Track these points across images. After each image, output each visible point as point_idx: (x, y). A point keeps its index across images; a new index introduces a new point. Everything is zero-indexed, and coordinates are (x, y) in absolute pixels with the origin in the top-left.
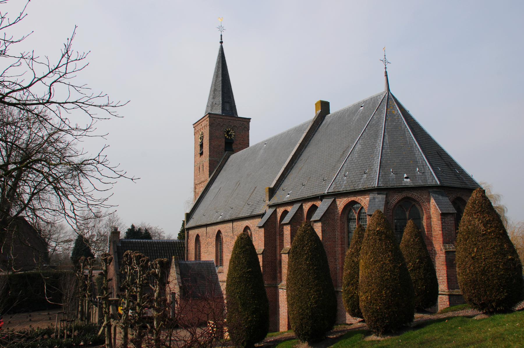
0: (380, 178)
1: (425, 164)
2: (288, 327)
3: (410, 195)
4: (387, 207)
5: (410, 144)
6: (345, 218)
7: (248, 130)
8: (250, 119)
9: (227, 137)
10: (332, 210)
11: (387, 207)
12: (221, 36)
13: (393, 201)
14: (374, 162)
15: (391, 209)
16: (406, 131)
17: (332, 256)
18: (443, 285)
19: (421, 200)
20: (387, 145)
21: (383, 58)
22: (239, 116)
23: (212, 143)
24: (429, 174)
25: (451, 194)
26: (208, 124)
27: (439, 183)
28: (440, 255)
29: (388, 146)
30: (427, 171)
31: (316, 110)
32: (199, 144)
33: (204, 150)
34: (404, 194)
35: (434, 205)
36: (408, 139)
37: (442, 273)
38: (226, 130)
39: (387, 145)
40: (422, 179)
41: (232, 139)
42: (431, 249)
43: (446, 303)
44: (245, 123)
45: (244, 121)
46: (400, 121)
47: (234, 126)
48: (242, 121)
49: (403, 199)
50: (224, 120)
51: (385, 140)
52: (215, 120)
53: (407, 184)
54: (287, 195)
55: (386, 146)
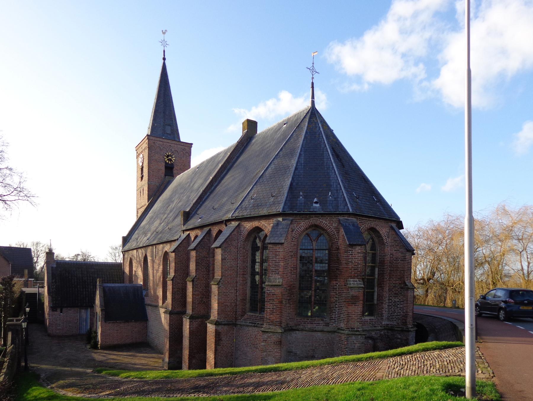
1: (339, 189)
2: (189, 357)
4: (292, 235)
5: (327, 165)
6: (249, 246)
7: (190, 155)
8: (192, 144)
9: (167, 161)
10: (235, 236)
11: (292, 235)
12: (164, 51)
13: (299, 229)
14: (284, 184)
15: (296, 238)
16: (325, 150)
17: (233, 287)
18: (344, 323)
19: (329, 229)
20: (301, 166)
21: (310, 66)
23: (151, 166)
24: (342, 199)
25: (364, 223)
26: (147, 147)
27: (351, 210)
28: (343, 291)
29: (302, 167)
30: (340, 197)
31: (243, 131)
32: (141, 167)
33: (144, 174)
34: (314, 220)
35: (342, 236)
36: (325, 160)
37: (344, 310)
38: (166, 154)
39: (301, 166)
41: (173, 164)
42: (336, 283)
43: (344, 343)
44: (186, 148)
45: (186, 146)
46: (320, 140)
48: (184, 146)
49: (310, 227)
50: (164, 143)
52: (154, 142)
53: (315, 210)
54: (199, 219)
55: (300, 167)
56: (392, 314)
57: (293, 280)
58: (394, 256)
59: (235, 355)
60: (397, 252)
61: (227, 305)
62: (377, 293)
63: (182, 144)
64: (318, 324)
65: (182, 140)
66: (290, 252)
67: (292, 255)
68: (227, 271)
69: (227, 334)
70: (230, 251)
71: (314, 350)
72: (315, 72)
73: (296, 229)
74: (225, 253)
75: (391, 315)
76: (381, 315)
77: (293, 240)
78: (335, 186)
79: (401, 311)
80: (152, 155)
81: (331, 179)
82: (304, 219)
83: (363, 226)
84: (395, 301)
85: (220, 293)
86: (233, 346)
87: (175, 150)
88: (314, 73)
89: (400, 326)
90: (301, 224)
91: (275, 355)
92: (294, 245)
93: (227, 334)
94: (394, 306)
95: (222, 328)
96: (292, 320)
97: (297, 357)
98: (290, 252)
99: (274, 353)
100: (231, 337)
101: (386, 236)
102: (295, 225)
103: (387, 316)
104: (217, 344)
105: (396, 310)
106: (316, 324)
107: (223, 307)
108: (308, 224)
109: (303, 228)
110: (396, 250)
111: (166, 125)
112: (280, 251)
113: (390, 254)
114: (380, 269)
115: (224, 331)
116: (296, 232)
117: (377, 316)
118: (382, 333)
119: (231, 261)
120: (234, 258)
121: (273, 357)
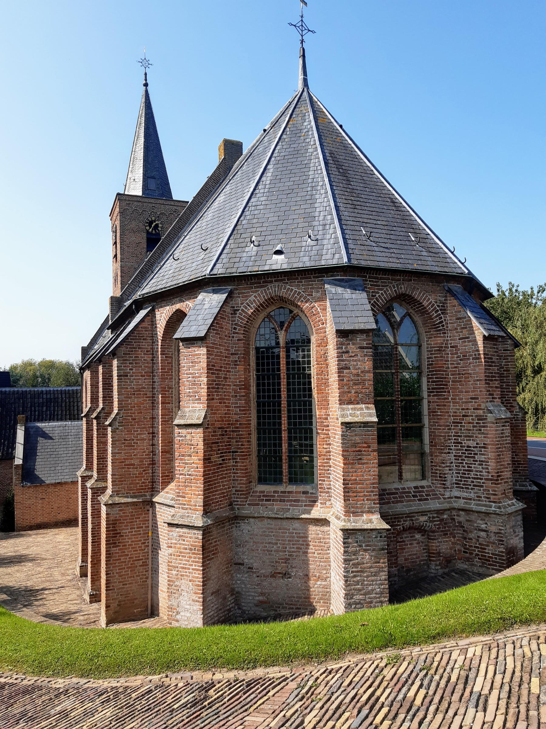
0: (223, 256)
3: (283, 293)
4: (235, 321)
10: (146, 331)
11: (235, 321)
12: (146, 74)
15: (241, 326)
17: (144, 428)
22: (174, 198)
40: (313, 253)
47: (161, 214)
51: (264, 179)
52: (129, 204)
56: (465, 474)
57: (240, 410)
58: (459, 349)
59: (152, 564)
60: (465, 342)
61: (134, 465)
62: (430, 429)
63: (176, 204)
64: (295, 501)
65: (174, 198)
66: (232, 354)
67: (236, 361)
68: (129, 398)
69: (132, 522)
70: (136, 360)
71: (288, 559)
72: (298, 25)
73: (242, 308)
74: (126, 363)
75: (464, 478)
76: (440, 477)
77: (237, 331)
78: (321, 218)
79: (483, 468)
80: (126, 223)
81: (317, 205)
82: (256, 287)
83: (380, 292)
84: (468, 447)
85: (116, 441)
86: (148, 546)
87: (161, 214)
88: (304, 32)
89: (482, 501)
90: (250, 298)
91: (193, 577)
92: (238, 340)
93: (132, 522)
94: (468, 457)
95: (120, 510)
96: (241, 495)
97: (255, 575)
98: (232, 354)
99: (191, 571)
100: (142, 527)
101: (438, 311)
102: (239, 301)
103: (454, 479)
104: (111, 544)
105: (473, 466)
106: (291, 501)
107: (123, 468)
108: (264, 296)
109: (254, 304)
110: (463, 338)
111: (148, 177)
112: (200, 355)
113: (451, 347)
114: (431, 378)
115: (126, 516)
116: (241, 314)
117: (432, 480)
118: (445, 516)
119: (139, 379)
120: (145, 373)
121: (190, 581)
